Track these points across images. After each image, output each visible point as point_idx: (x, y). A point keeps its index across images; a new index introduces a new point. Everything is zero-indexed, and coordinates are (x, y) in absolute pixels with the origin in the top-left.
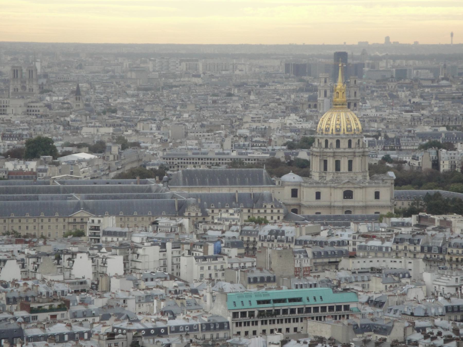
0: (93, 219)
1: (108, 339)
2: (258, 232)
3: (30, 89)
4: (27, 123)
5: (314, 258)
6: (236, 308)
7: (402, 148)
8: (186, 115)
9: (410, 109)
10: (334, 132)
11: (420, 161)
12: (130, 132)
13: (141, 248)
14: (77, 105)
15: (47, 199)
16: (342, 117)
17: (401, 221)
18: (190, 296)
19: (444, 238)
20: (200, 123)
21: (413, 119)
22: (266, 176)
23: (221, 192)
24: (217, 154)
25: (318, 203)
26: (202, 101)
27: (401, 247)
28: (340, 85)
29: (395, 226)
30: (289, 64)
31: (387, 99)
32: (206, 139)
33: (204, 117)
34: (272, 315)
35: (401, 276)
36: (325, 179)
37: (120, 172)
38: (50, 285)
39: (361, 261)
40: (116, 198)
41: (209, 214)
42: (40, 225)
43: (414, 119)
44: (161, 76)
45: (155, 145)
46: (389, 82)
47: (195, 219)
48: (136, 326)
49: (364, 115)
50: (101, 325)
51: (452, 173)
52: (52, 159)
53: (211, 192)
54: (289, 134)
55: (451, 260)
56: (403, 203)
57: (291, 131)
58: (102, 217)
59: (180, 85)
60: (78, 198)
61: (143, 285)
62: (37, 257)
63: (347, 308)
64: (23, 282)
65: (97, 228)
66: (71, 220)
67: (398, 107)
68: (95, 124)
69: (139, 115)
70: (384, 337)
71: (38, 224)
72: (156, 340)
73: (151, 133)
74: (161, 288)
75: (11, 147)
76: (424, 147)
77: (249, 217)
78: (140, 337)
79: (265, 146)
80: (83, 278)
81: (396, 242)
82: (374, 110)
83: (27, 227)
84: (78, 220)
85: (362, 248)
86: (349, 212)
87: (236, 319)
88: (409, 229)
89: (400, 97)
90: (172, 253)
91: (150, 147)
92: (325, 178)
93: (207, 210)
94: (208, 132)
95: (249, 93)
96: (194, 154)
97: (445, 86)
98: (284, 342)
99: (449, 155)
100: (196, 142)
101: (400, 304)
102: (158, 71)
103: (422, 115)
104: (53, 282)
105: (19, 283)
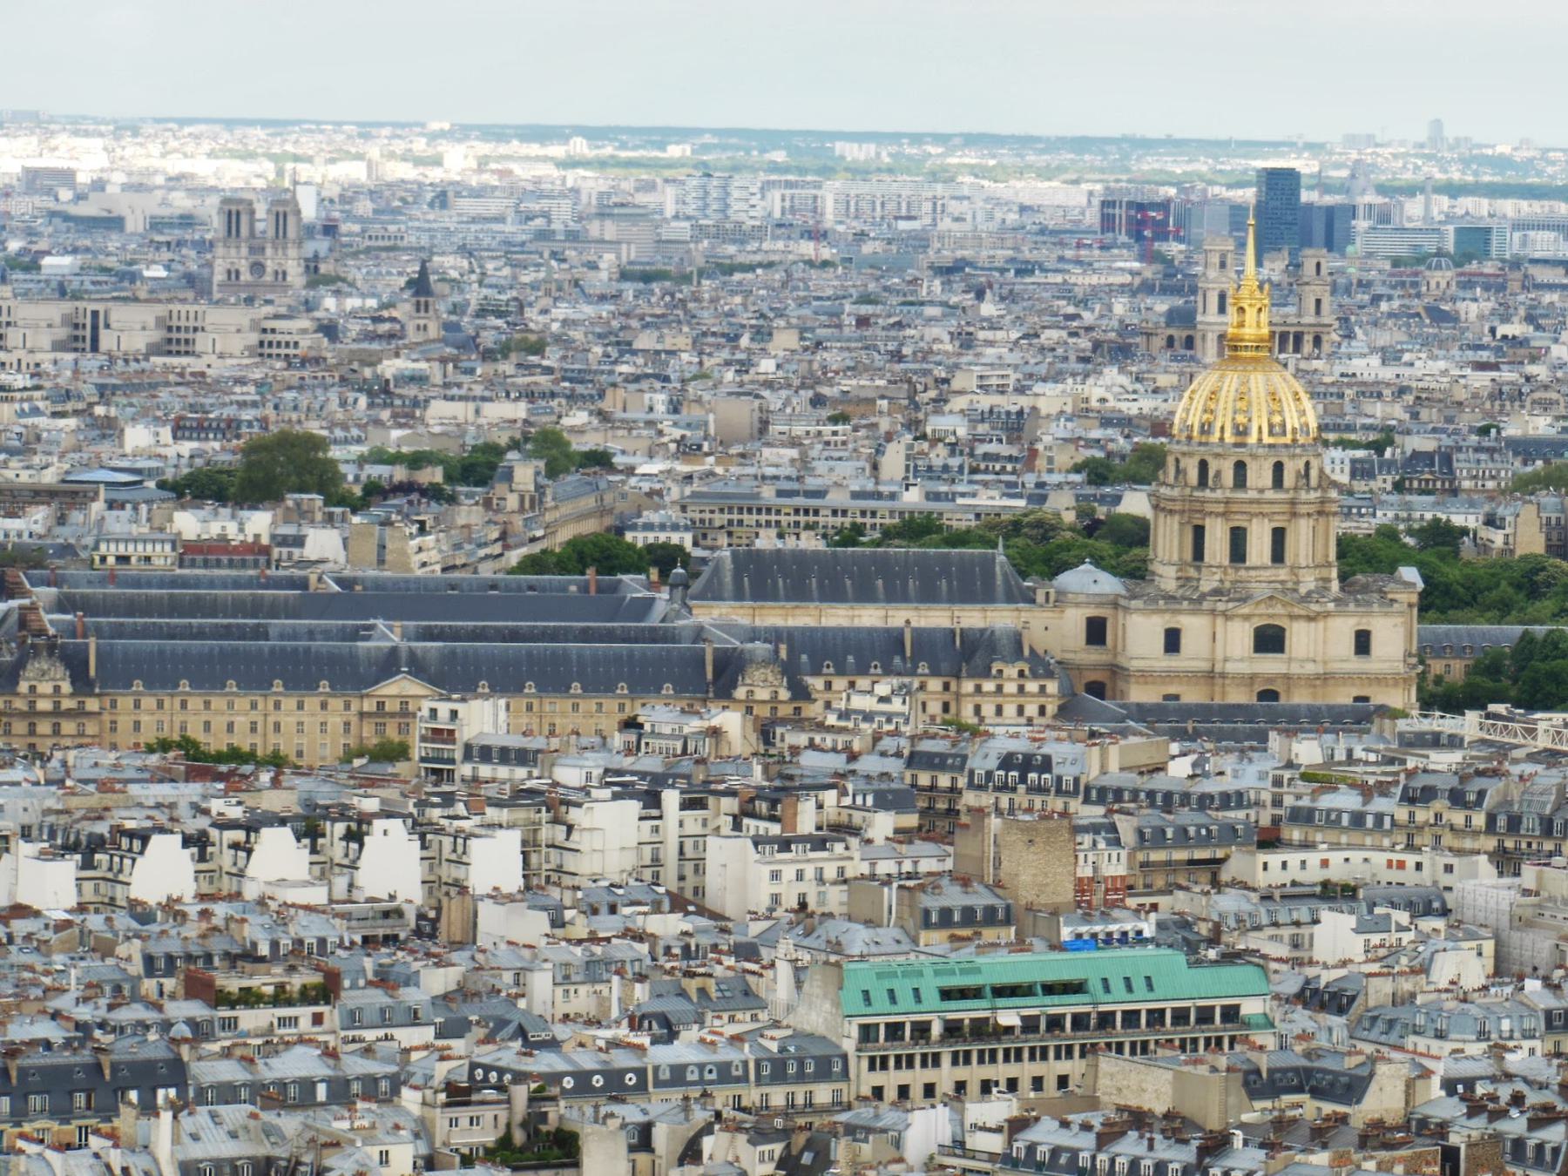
0: (434, 705)
2: (965, 758)
3: (276, 273)
5: (1142, 848)
6: (869, 1010)
8: (767, 366)
9: (1493, 360)
11: (1508, 530)
13: (579, 805)
14: (418, 327)
15: (294, 636)
18: (729, 968)
20: (810, 393)
21: (1497, 394)
22: (1005, 575)
23: (857, 623)
24: (856, 495)
25: (1173, 662)
26: (823, 318)
27: (1422, 815)
29: (1411, 745)
31: (1421, 325)
32: (828, 443)
33: (825, 374)
37: (536, 549)
42: (271, 719)
43: (1501, 393)
44: (700, 232)
46: (1429, 268)
48: (545, 1062)
49: (1342, 375)
50: (436, 1055)
54: (1096, 434)
57: (1106, 422)
58: (463, 700)
59: (760, 265)
60: (389, 634)
63: (1231, 1014)
64: (199, 907)
66: (369, 706)
67: (1455, 352)
69: (615, 362)
73: (650, 424)
74: (639, 937)
75: (199, 462)
78: (553, 1099)
79: (1014, 472)
80: (392, 897)
82: (1375, 361)
83: (230, 727)
85: (1302, 817)
88: (1455, 757)
89: (1463, 317)
90: (681, 825)
94: (834, 420)
95: (980, 295)
100: (794, 453)
101: (1403, 1003)
102: (688, 218)
103: (1528, 379)
104: (292, 911)
105: (186, 909)
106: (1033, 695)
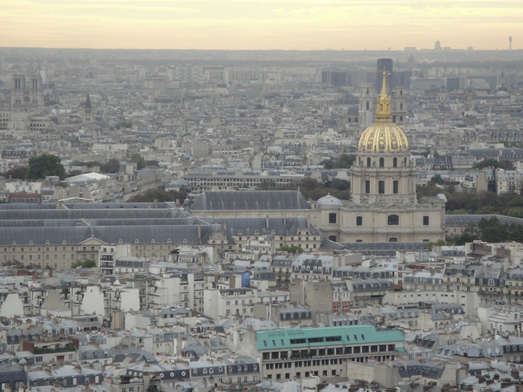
0: (105, 247)
1: (122, 383)
2: (291, 262)
3: (34, 101)
4: (30, 138)
5: (355, 292)
6: (266, 348)
7: (454, 167)
8: (210, 130)
9: (463, 123)
10: (377, 149)
11: (474, 182)
12: (147, 149)
13: (159, 280)
14: (87, 119)
15: (53, 225)
16: (386, 132)
17: (453, 250)
18: (215, 335)
19: (502, 269)
20: (226, 139)
21: (467, 134)
22: (300, 199)
23: (249, 217)
24: (245, 174)
25: (359, 229)
26: (228, 114)
27: (453, 279)
28: (384, 96)
29: (446, 255)
30: (326, 73)
31: (437, 112)
32: (233, 157)
33: (230, 133)
34: (307, 356)
35: (453, 311)
36: (367, 203)
37: (135, 194)
38: (56, 322)
39: (408, 294)
40: (131, 223)
41: (236, 242)
42: (45, 254)
43: (468, 135)
44: (181, 86)
45: (175, 164)
47: (220, 247)
48: (154, 368)
49: (411, 130)
50: (115, 367)
51: (510, 196)
52: (58, 179)
53: (238, 217)
54: (326, 152)
55: (510, 293)
56: (455, 229)
57: (329, 148)
58: (115, 245)
59: (204, 96)
60: (88, 224)
61: (161, 322)
62: (42, 290)
63: (392, 348)
64: (26, 319)
65: (110, 258)
66: (80, 249)
67: (450, 121)
68: (107, 140)
70: (433, 380)
71: (43, 253)
72: (176, 384)
73: (171, 151)
74: (182, 325)
75: (12, 166)
76: (479, 167)
77: (281, 245)
79: (299, 165)
80: (94, 314)
81: (448, 273)
82: (422, 125)
83: (31, 257)
84: (88, 249)
85: (408, 280)
86: (394, 239)
87: (267, 360)
88: (462, 259)
89: (452, 109)
90: (195, 286)
91: (170, 166)
92: (367, 201)
93: (234, 237)
94: (235, 149)
95: (282, 106)
96: (219, 174)
97: (503, 98)
98: (321, 387)
99: (507, 175)
100: (222, 160)
101: (451, 344)
102: (178, 81)
103: (477, 130)
104: (60, 319)
105: (21, 319)
106: (312, 241)
